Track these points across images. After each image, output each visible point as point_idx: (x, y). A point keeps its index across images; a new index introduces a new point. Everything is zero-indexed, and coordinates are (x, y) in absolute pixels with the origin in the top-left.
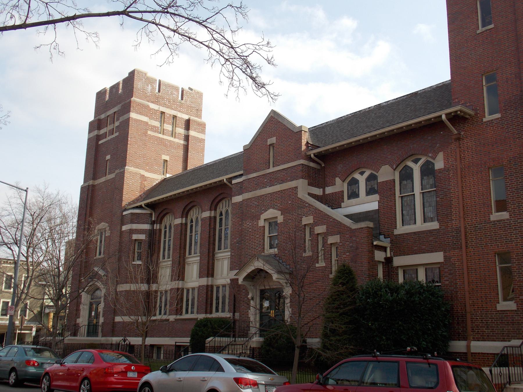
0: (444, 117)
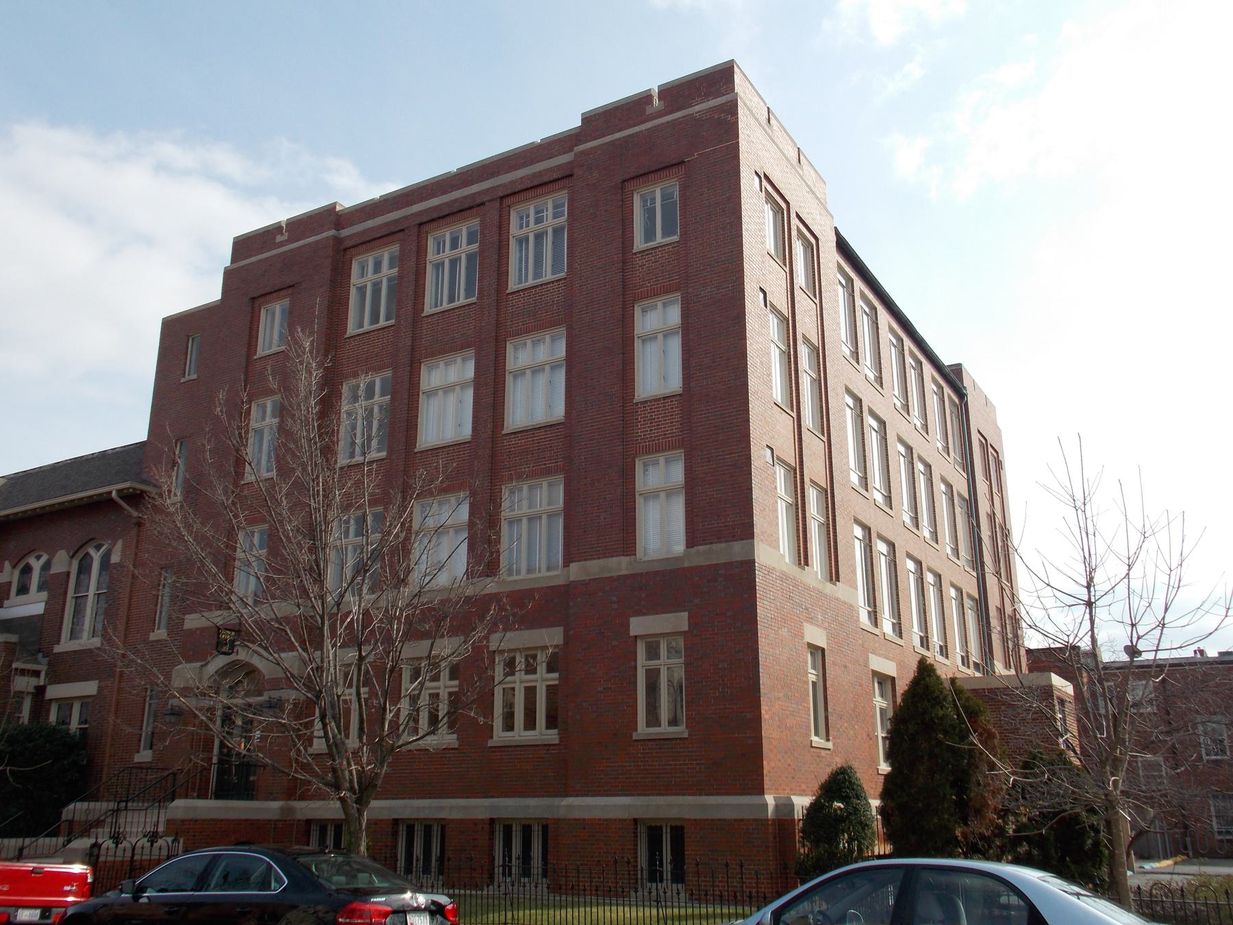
0: (114, 494)
